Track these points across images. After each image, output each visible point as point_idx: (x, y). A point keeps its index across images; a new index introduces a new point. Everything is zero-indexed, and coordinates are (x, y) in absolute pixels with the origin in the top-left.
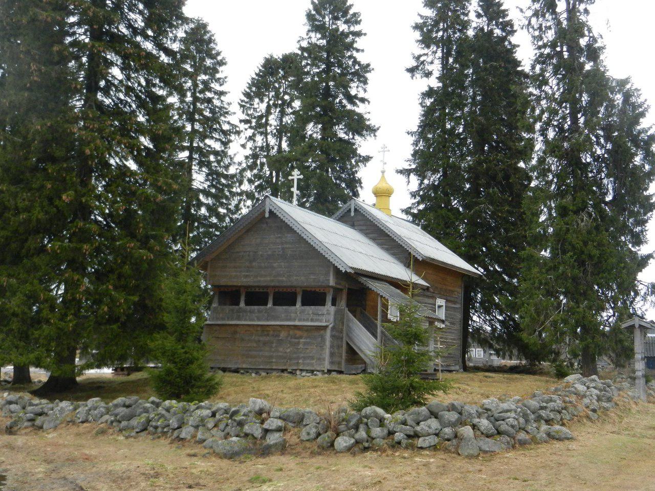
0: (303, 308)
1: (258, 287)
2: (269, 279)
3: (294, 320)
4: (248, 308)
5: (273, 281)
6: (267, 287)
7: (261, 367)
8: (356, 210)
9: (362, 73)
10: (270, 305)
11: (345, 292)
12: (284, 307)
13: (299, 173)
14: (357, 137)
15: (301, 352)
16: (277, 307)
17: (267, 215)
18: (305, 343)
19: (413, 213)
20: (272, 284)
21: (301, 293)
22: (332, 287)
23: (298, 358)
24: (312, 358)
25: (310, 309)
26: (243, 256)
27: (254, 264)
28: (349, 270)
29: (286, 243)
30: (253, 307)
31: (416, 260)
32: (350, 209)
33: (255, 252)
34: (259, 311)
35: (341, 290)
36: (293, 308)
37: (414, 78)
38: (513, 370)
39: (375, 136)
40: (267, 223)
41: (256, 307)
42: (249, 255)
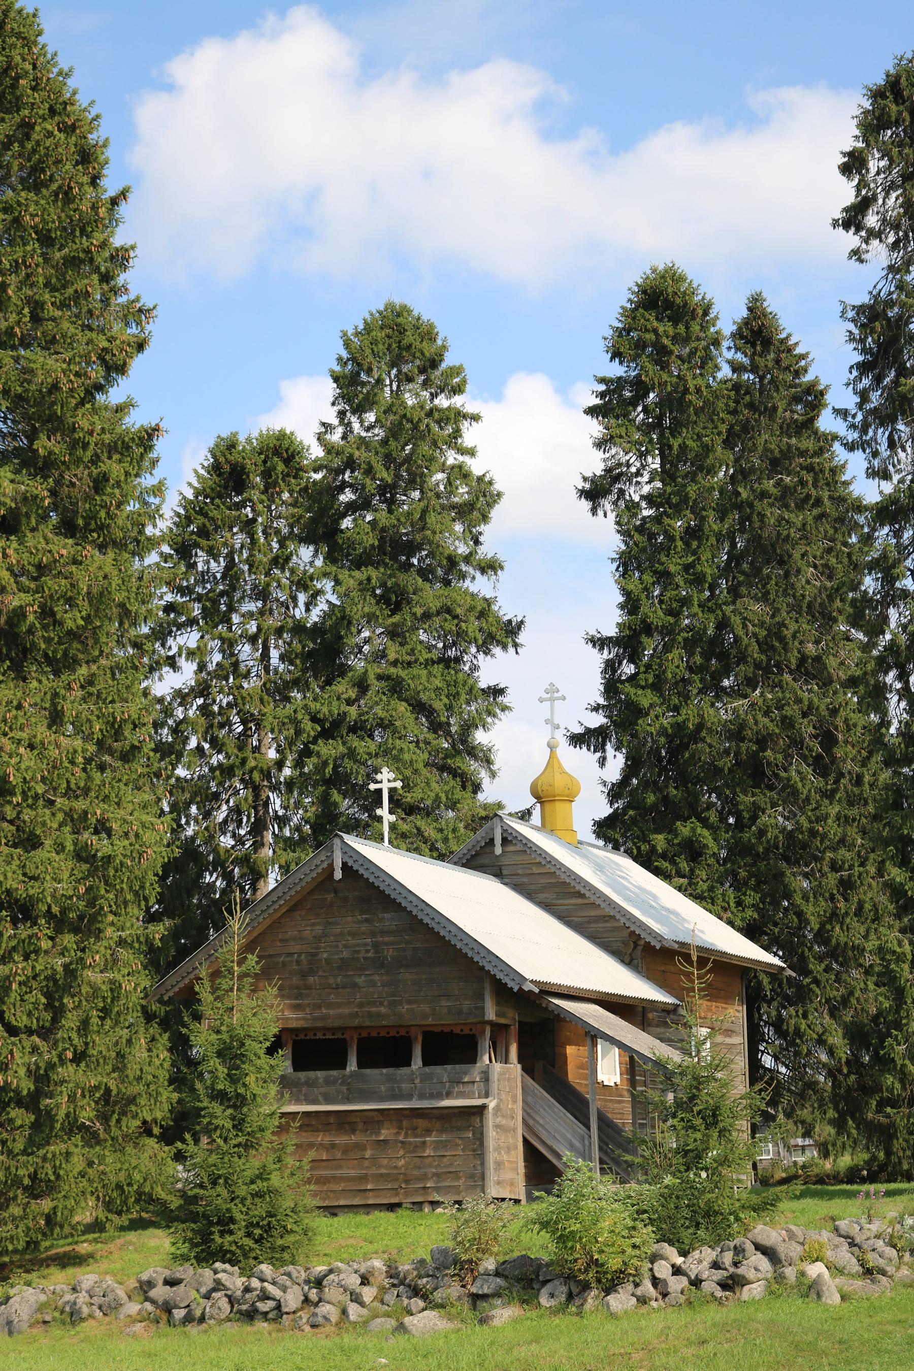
0: (427, 1069)
1: (324, 1029)
2: (346, 1011)
3: (409, 1097)
4: (302, 1075)
5: (356, 1015)
6: (343, 1029)
7: (342, 1203)
8: (505, 841)
9: (479, 502)
10: (352, 1065)
11: (514, 1030)
12: (384, 1071)
13: (392, 776)
14: (481, 656)
15: (430, 1166)
16: (368, 1071)
17: (338, 875)
18: (438, 1145)
19: (344, 516)
20: (356, 1022)
21: (420, 1038)
22: (491, 1023)
23: (424, 1178)
24: (455, 1175)
25: (442, 1072)
26: (284, 965)
27: (311, 979)
28: (528, 987)
29: (382, 932)
30: (311, 1074)
31: (648, 947)
32: (492, 840)
33: (314, 955)
34: (328, 1082)
35: (506, 1027)
36: (404, 1071)
37: (600, 513)
38: (852, 1176)
39: (516, 645)
40: (336, 891)
41: (320, 1074)
42: (298, 962)
